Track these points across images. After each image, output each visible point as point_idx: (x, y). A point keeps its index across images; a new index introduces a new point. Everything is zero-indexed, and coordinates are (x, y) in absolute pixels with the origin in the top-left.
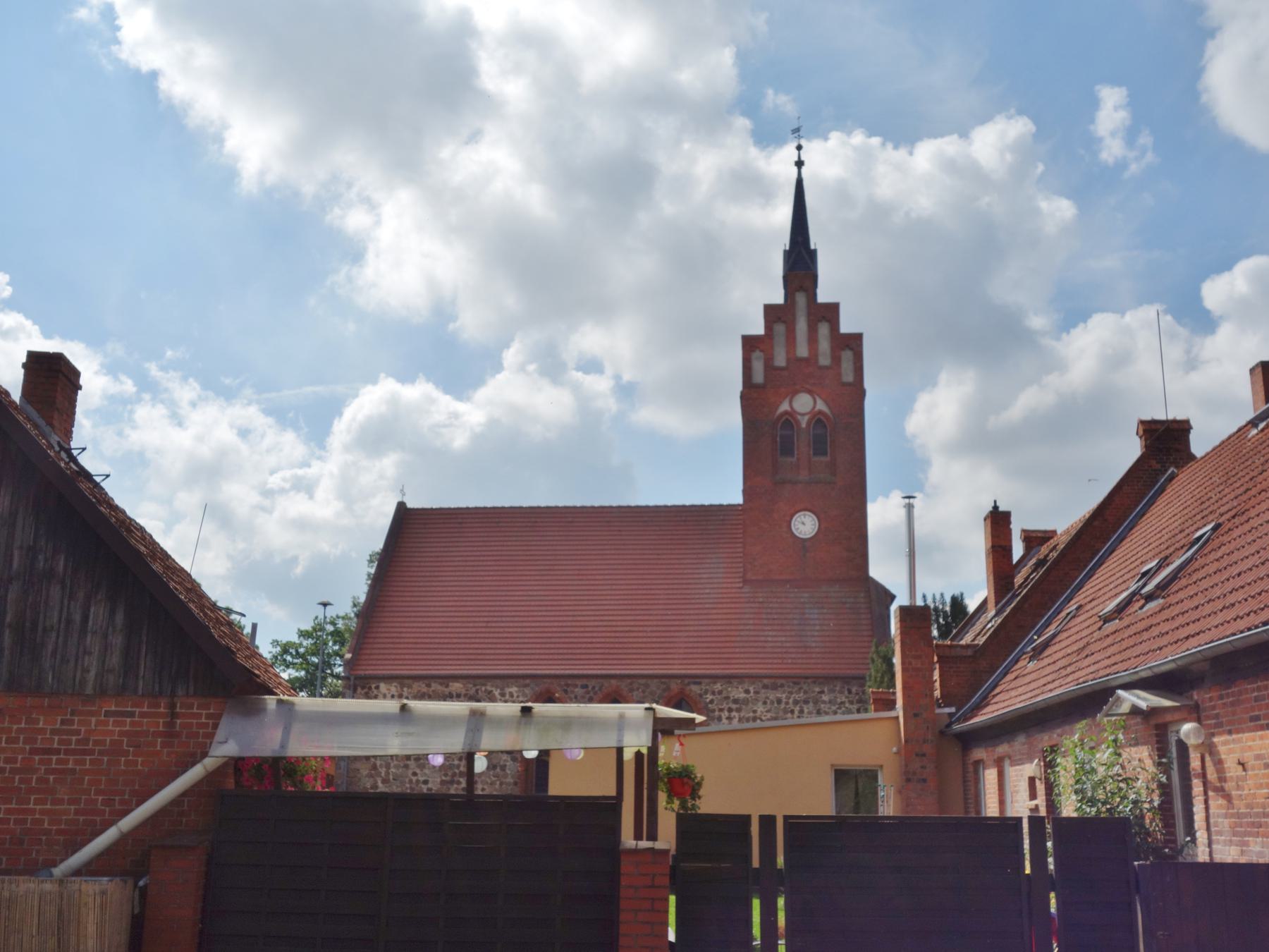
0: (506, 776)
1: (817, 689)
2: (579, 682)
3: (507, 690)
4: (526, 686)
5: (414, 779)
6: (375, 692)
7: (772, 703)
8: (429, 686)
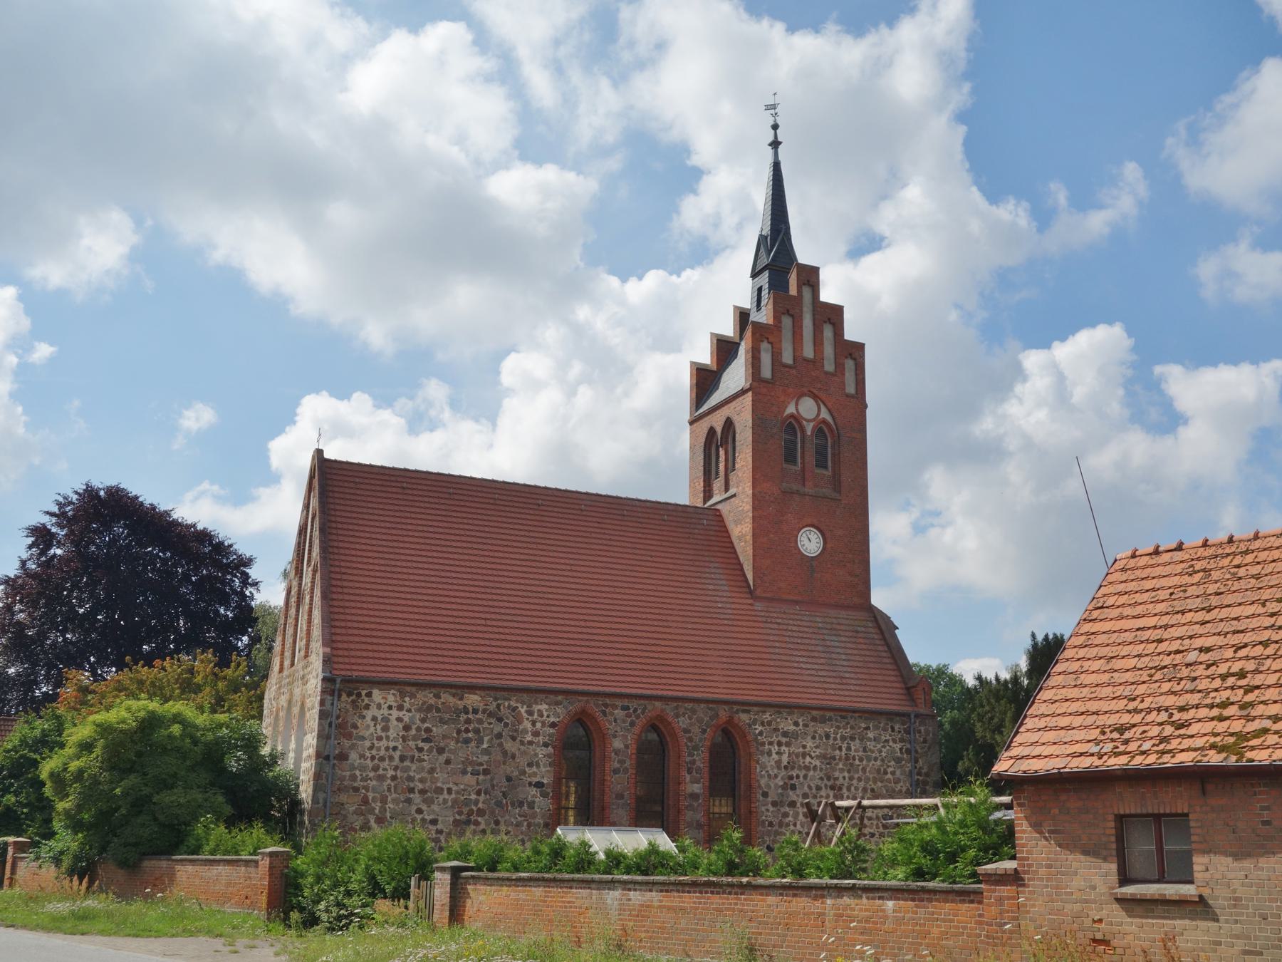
0: (534, 816)
1: (863, 725)
2: (619, 703)
3: (536, 708)
4: (558, 703)
5: (419, 817)
6: (366, 700)
7: (821, 738)
8: (437, 696)
